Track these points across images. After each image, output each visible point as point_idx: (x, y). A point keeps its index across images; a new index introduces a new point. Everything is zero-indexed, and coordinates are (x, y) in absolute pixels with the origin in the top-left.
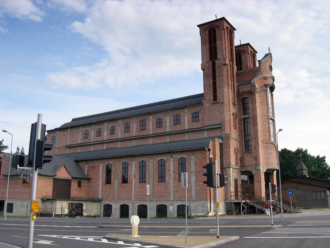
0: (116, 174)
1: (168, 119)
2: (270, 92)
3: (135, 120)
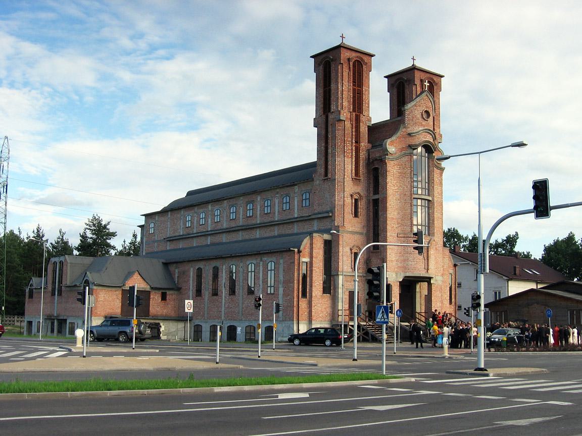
0: (207, 283)
2: (427, 154)
3: (242, 202)
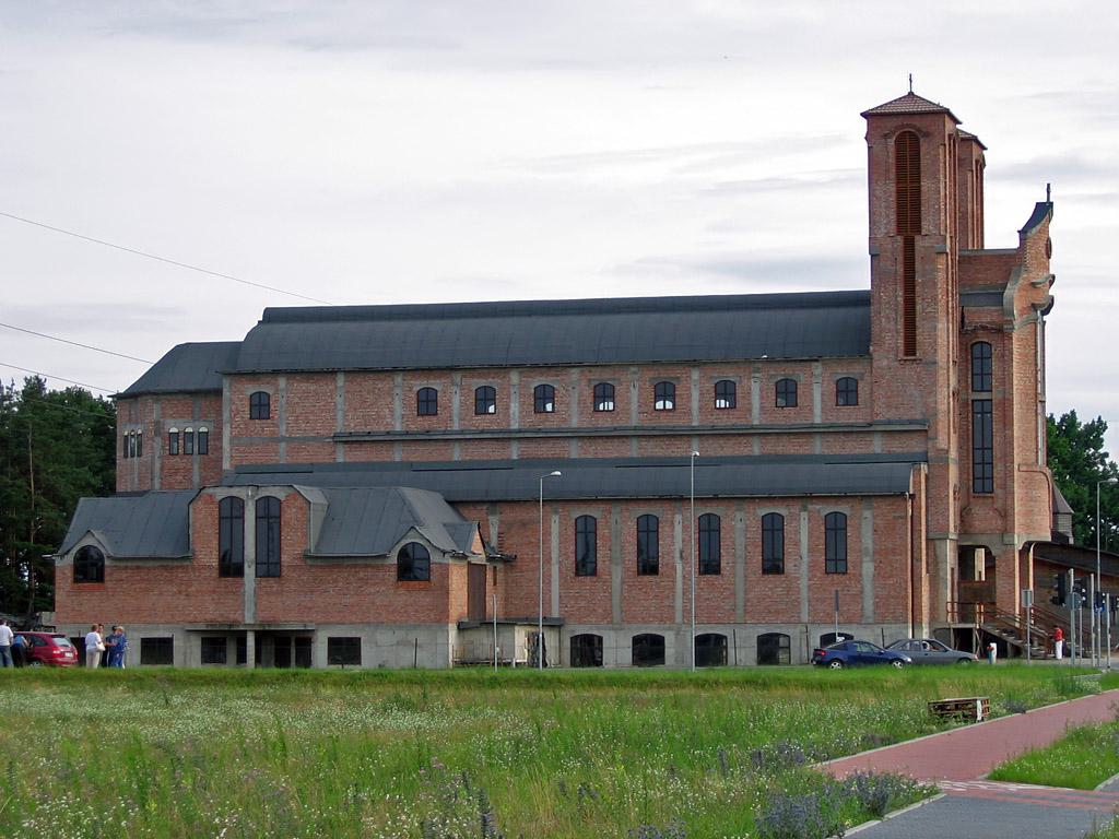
1: (755, 387)
